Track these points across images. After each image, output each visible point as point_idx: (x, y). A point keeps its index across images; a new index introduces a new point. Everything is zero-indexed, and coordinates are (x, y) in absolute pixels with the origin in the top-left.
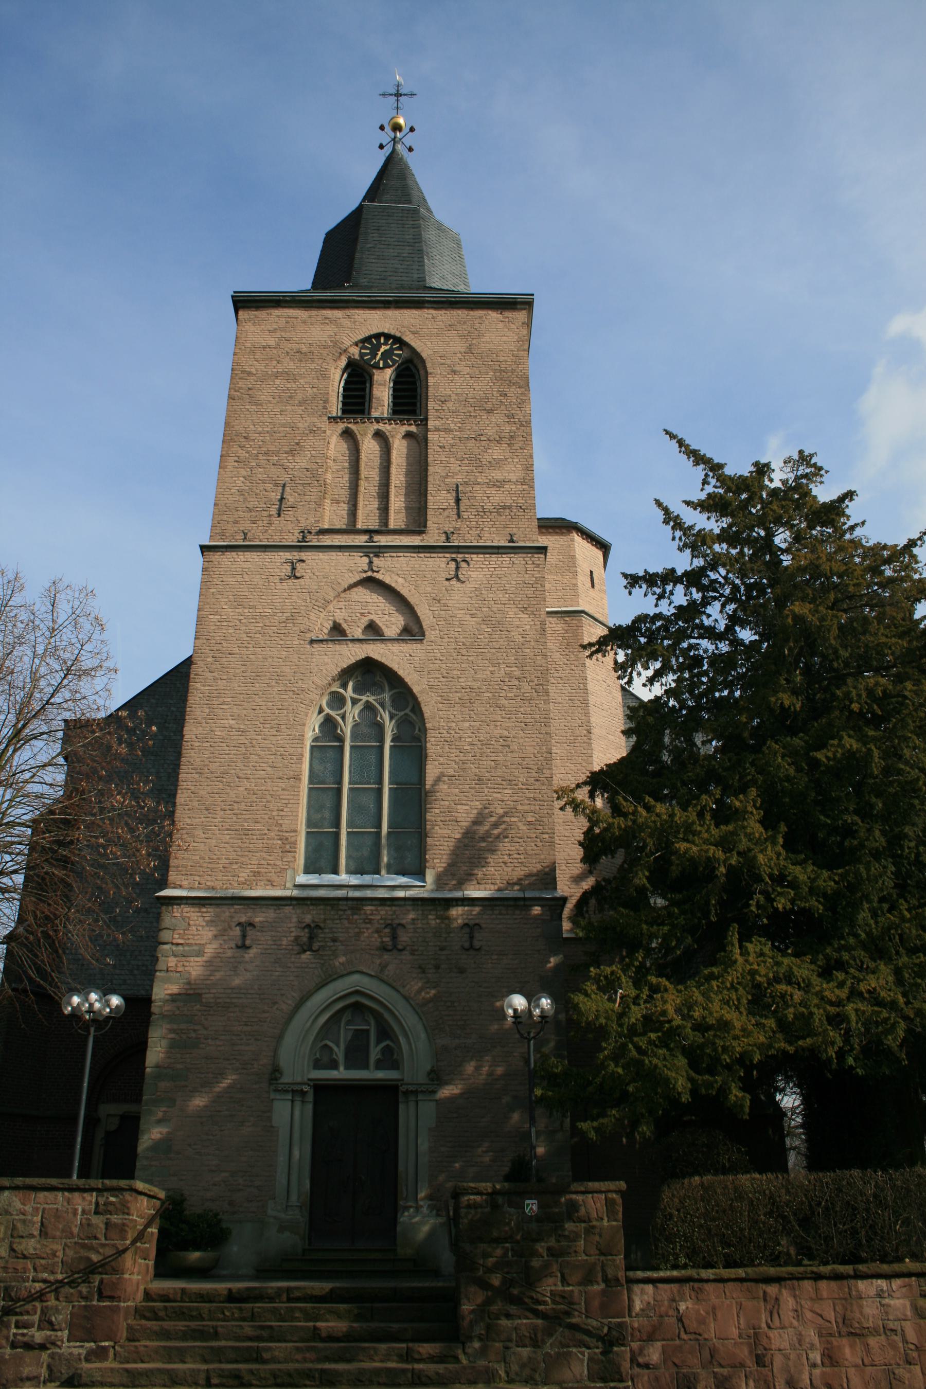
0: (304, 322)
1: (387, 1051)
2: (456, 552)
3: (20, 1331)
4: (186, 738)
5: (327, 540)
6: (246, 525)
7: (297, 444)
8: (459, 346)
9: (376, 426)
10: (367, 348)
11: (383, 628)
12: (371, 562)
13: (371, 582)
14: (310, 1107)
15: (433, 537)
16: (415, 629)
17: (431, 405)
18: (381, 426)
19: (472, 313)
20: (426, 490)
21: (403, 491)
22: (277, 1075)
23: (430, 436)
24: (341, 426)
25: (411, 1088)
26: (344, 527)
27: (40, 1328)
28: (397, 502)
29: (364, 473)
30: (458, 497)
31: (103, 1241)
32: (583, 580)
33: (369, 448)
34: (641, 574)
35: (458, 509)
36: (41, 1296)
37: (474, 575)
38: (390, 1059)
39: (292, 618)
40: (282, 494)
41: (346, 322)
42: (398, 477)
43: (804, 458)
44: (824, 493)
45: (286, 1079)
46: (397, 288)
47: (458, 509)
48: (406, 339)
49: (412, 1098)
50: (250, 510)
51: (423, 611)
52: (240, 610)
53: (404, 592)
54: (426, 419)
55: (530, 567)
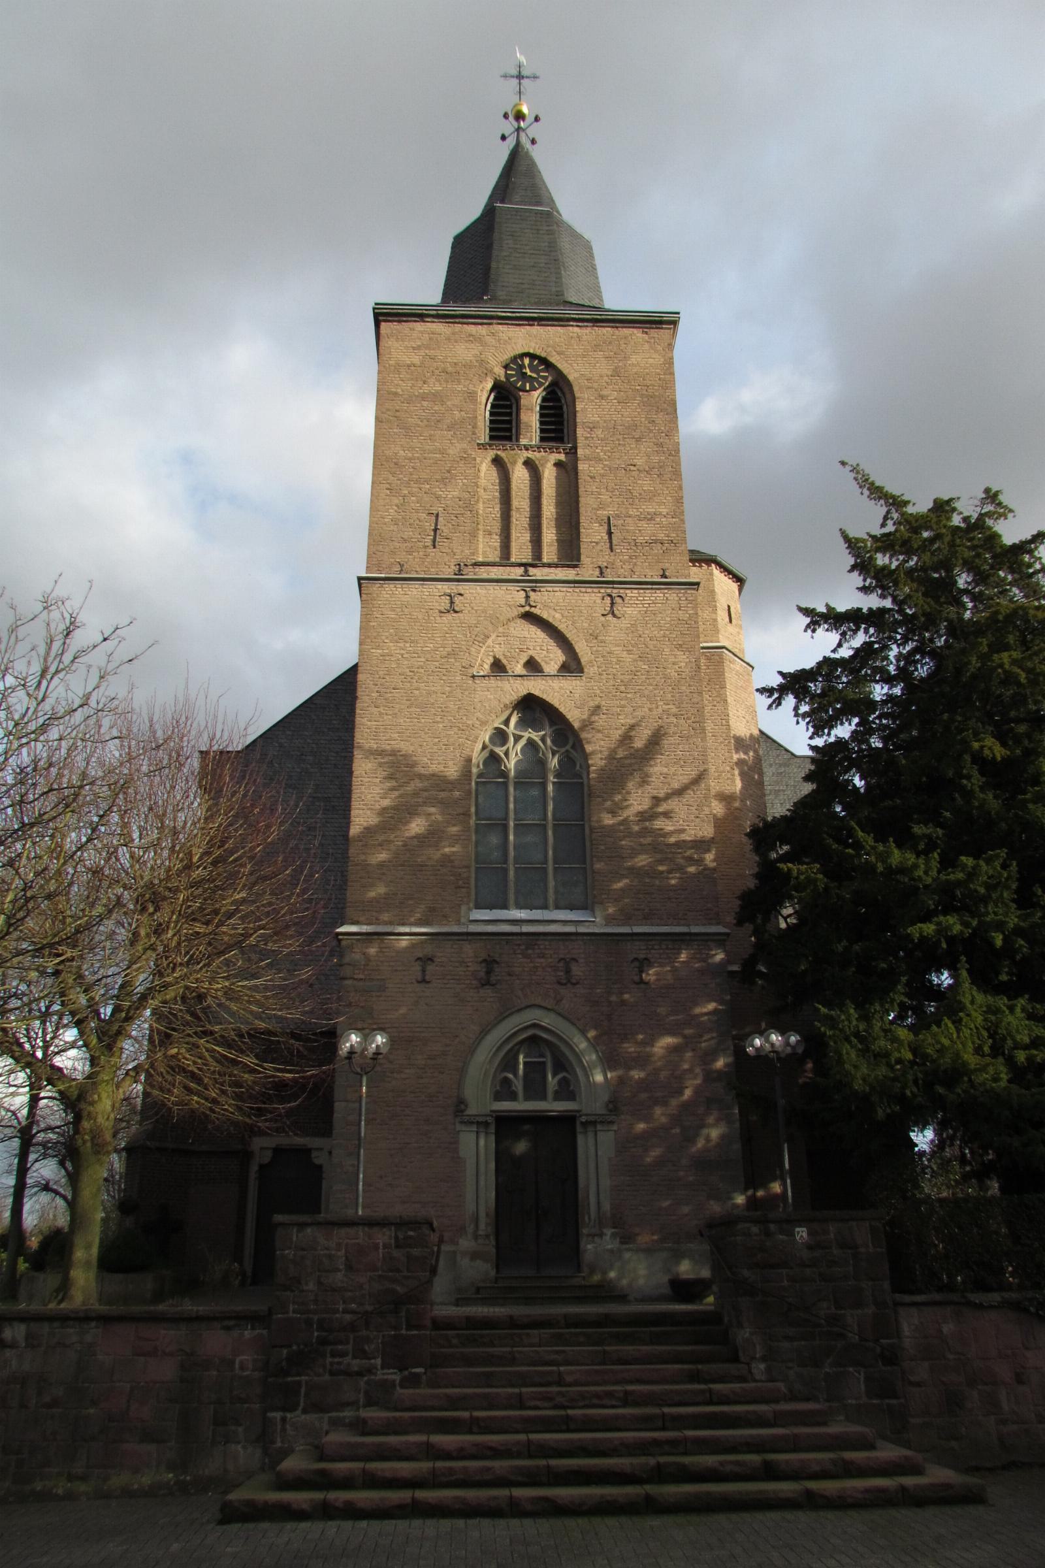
0: (448, 339)
1: (564, 1083)
2: (609, 586)
3: (336, 1360)
4: (356, 773)
5: (483, 573)
6: (401, 557)
7: (449, 472)
8: (604, 368)
9: (526, 454)
10: (512, 369)
11: (543, 664)
12: (527, 597)
13: (530, 617)
14: (493, 1138)
15: (588, 572)
16: (573, 666)
17: (579, 431)
18: (530, 454)
19: (616, 331)
20: (578, 523)
21: (553, 523)
22: (463, 1107)
23: (582, 466)
24: (491, 454)
25: (592, 1118)
26: (498, 560)
27: (354, 1357)
28: (549, 535)
29: (515, 503)
30: (609, 529)
31: (405, 1273)
32: (722, 615)
33: (520, 476)
34: (822, 609)
35: (611, 542)
36: (353, 1327)
37: (629, 610)
38: (566, 1091)
39: (452, 654)
40: (436, 524)
41: (490, 340)
42: (549, 509)
43: (991, 496)
44: (1011, 532)
45: (469, 1112)
46: (536, 303)
47: (611, 542)
48: (552, 360)
49: (591, 1128)
50: (405, 541)
51: (581, 647)
52: (401, 645)
53: (562, 627)
54: (575, 448)
55: (683, 603)
